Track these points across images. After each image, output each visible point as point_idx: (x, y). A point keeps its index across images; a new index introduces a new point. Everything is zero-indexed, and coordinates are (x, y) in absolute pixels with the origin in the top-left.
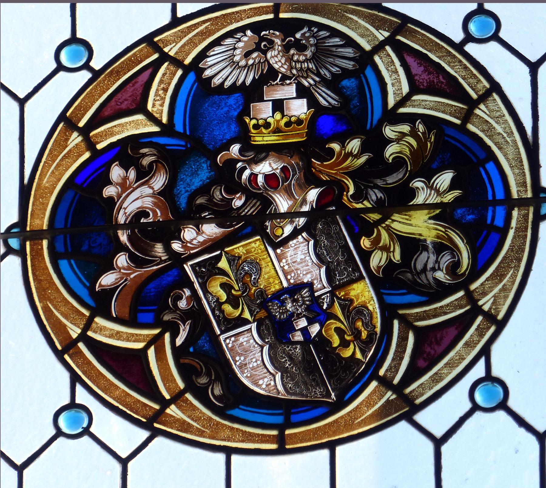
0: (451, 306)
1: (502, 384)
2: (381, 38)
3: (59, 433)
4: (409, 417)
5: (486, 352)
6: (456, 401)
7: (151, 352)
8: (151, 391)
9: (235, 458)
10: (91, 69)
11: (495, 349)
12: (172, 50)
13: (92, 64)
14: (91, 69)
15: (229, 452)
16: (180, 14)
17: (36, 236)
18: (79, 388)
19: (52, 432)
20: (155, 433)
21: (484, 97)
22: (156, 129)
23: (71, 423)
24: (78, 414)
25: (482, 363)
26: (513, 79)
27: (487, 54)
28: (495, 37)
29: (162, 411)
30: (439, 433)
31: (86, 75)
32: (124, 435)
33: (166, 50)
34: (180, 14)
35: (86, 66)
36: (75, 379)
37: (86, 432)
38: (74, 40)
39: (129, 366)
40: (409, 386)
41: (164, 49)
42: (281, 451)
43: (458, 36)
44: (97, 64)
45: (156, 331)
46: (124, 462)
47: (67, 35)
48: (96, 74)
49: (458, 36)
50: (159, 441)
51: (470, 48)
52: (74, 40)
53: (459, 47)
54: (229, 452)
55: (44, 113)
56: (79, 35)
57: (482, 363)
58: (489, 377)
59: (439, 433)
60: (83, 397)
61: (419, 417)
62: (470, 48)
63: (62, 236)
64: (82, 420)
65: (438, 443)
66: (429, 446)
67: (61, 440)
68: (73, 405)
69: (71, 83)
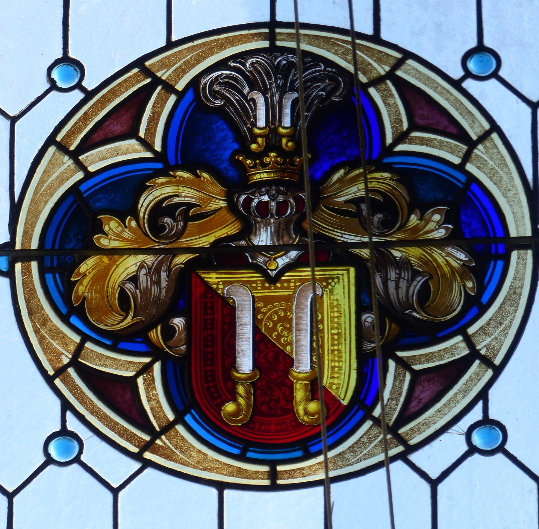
0: (454, 347)
1: (503, 429)
2: (383, 73)
3: (49, 461)
4: (403, 457)
5: (483, 396)
6: (453, 444)
7: (140, 381)
8: (142, 422)
9: (228, 493)
10: (83, 90)
11: (492, 393)
12: (164, 74)
13: (84, 84)
14: (463, 79)
15: (221, 487)
16: (174, 38)
17: (26, 256)
18: (69, 414)
19: (42, 459)
20: (147, 464)
21: (484, 137)
22: (149, 155)
23: (62, 448)
24: (70, 443)
25: (480, 405)
26: (514, 121)
27: (487, 92)
28: (495, 75)
29: (152, 441)
30: (434, 475)
31: (77, 96)
32: (116, 466)
33: (159, 74)
34: (174, 38)
35: (79, 86)
36: (66, 406)
37: (77, 460)
38: (66, 59)
39: (119, 394)
40: (154, 428)
41: (157, 74)
42: (274, 487)
43: (457, 73)
44: (90, 84)
45: (147, 360)
46: (115, 492)
47: (473, 43)
48: (89, 95)
49: (457, 73)
50: (149, 471)
51: (469, 85)
52: (66, 59)
53: (457, 84)
54: (221, 487)
55: (33, 133)
56: (72, 54)
57: (480, 405)
58: (486, 421)
59: (434, 475)
60: (73, 424)
61: (414, 457)
62: (469, 85)
63: (49, 257)
64: (72, 449)
65: (434, 484)
66: (426, 487)
67: (51, 468)
68: (64, 432)
69: (62, 104)
